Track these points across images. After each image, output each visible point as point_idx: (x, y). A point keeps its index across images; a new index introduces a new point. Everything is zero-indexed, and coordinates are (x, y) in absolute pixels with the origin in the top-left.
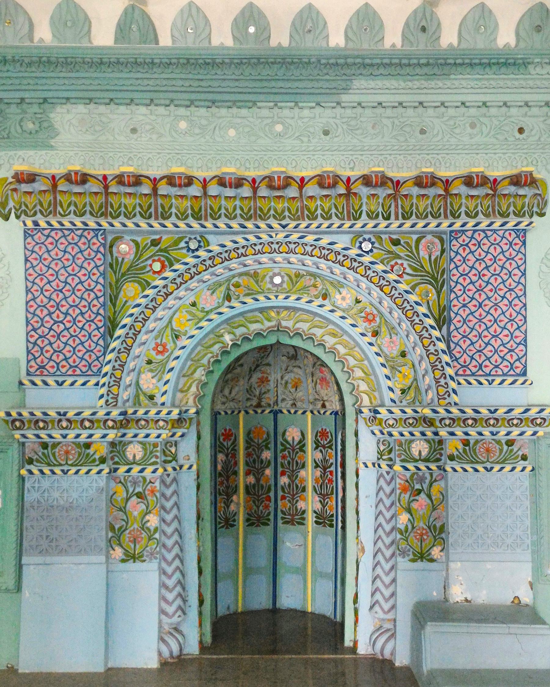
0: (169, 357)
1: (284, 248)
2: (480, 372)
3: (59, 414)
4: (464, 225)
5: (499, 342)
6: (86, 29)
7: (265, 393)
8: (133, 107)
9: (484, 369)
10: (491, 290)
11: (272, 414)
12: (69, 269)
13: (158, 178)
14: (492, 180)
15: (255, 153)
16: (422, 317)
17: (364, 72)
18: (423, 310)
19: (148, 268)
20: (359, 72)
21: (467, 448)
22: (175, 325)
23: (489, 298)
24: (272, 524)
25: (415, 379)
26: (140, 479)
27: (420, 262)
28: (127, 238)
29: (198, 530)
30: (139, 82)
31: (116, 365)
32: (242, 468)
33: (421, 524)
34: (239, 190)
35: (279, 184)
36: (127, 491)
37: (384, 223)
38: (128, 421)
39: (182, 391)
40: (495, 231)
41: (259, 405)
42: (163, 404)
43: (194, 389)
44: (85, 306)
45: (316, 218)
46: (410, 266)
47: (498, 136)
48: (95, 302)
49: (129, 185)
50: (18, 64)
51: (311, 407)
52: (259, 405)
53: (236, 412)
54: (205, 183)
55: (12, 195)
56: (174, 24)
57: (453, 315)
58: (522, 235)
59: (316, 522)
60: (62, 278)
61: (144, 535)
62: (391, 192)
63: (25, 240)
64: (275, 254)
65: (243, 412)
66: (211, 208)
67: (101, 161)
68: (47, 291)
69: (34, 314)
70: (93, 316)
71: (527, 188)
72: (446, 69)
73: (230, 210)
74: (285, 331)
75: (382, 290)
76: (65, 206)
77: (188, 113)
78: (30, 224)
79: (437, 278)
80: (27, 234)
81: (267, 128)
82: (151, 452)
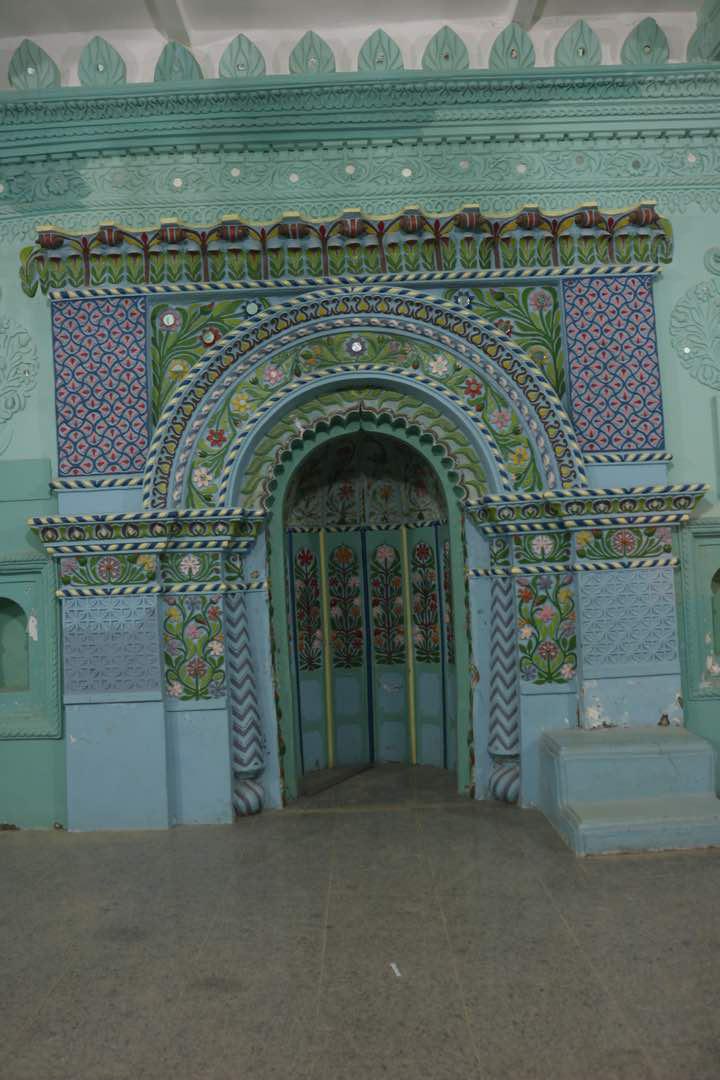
0: (227, 446)
2: (610, 448)
6: (120, 74)
8: (176, 157)
9: (614, 444)
10: (617, 349)
11: (359, 533)
13: (207, 232)
14: (607, 220)
15: (323, 199)
17: (448, 99)
19: (199, 341)
21: (600, 541)
23: (614, 358)
24: (365, 664)
25: (533, 460)
26: (200, 600)
27: (529, 319)
29: (273, 662)
30: (183, 124)
31: (163, 456)
32: (325, 599)
33: (548, 639)
34: (304, 242)
35: (356, 230)
36: (184, 616)
37: (482, 273)
38: (180, 527)
41: (342, 522)
42: (222, 505)
43: (260, 489)
44: (124, 390)
45: (401, 269)
46: (518, 324)
47: (609, 172)
48: (136, 384)
49: (173, 242)
50: (42, 114)
51: (406, 520)
52: (342, 522)
53: (315, 530)
54: (263, 235)
55: (38, 266)
56: (222, 62)
57: (574, 379)
58: (649, 281)
59: (419, 659)
62: (488, 235)
63: (53, 315)
65: (323, 530)
66: (272, 265)
67: (141, 220)
68: (78, 374)
69: (65, 403)
72: (544, 93)
73: (296, 266)
74: (369, 417)
75: (486, 352)
76: (99, 273)
77: (241, 159)
78: (57, 295)
79: (553, 340)
80: (55, 307)
81: (336, 171)
82: (210, 566)
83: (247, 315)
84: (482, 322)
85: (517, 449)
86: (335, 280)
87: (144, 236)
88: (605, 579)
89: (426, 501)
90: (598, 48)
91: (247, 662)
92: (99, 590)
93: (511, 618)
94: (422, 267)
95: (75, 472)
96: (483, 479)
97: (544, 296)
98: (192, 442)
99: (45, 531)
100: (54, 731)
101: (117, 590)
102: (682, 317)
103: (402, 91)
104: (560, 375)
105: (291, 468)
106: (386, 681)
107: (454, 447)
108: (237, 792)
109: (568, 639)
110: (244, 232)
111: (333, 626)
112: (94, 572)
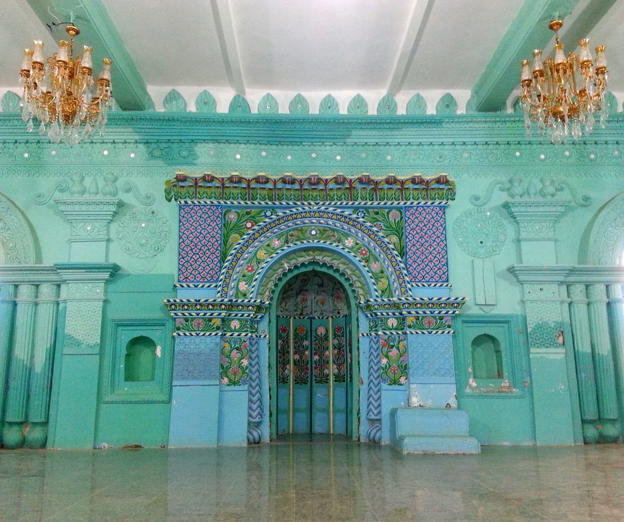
0: (255, 273)
1: (317, 215)
2: (424, 280)
3: (196, 300)
4: (412, 203)
5: (433, 264)
7: (305, 307)
11: (309, 320)
12: (202, 226)
14: (426, 181)
16: (391, 250)
18: (391, 246)
19: (244, 226)
20: (355, 127)
22: (258, 257)
23: (426, 241)
24: (309, 383)
25: (389, 285)
28: (233, 210)
30: (242, 131)
32: (292, 351)
33: (394, 365)
35: (315, 182)
37: (370, 203)
39: (261, 294)
40: (428, 207)
42: (252, 298)
43: (267, 293)
44: (210, 246)
46: (384, 225)
49: (236, 183)
52: (301, 314)
54: (275, 182)
56: (259, 104)
57: (408, 250)
58: (443, 208)
59: (335, 381)
60: (199, 231)
61: (240, 371)
62: (373, 186)
64: (312, 218)
65: (292, 318)
67: (221, 172)
70: (215, 251)
71: (444, 185)
72: (400, 126)
73: (288, 196)
74: (317, 263)
78: (183, 202)
80: (181, 207)
82: (244, 325)
83: (266, 217)
84: (369, 224)
85: (382, 280)
86: (306, 203)
87: (223, 179)
88: (421, 338)
89: (341, 305)
90: (426, 105)
91: (258, 370)
92: (193, 333)
93: (378, 355)
94: (213, 197)
95: (186, 280)
96: (368, 292)
97: (396, 213)
98: (239, 270)
99: (171, 305)
100: (164, 398)
101: (202, 334)
102: (459, 224)
103: (338, 123)
104: (402, 248)
105: (281, 285)
106: (319, 393)
107: (355, 278)
108: (249, 432)
109: (404, 365)
110: (267, 181)
111: (295, 364)
112: (192, 325)
